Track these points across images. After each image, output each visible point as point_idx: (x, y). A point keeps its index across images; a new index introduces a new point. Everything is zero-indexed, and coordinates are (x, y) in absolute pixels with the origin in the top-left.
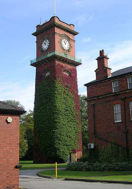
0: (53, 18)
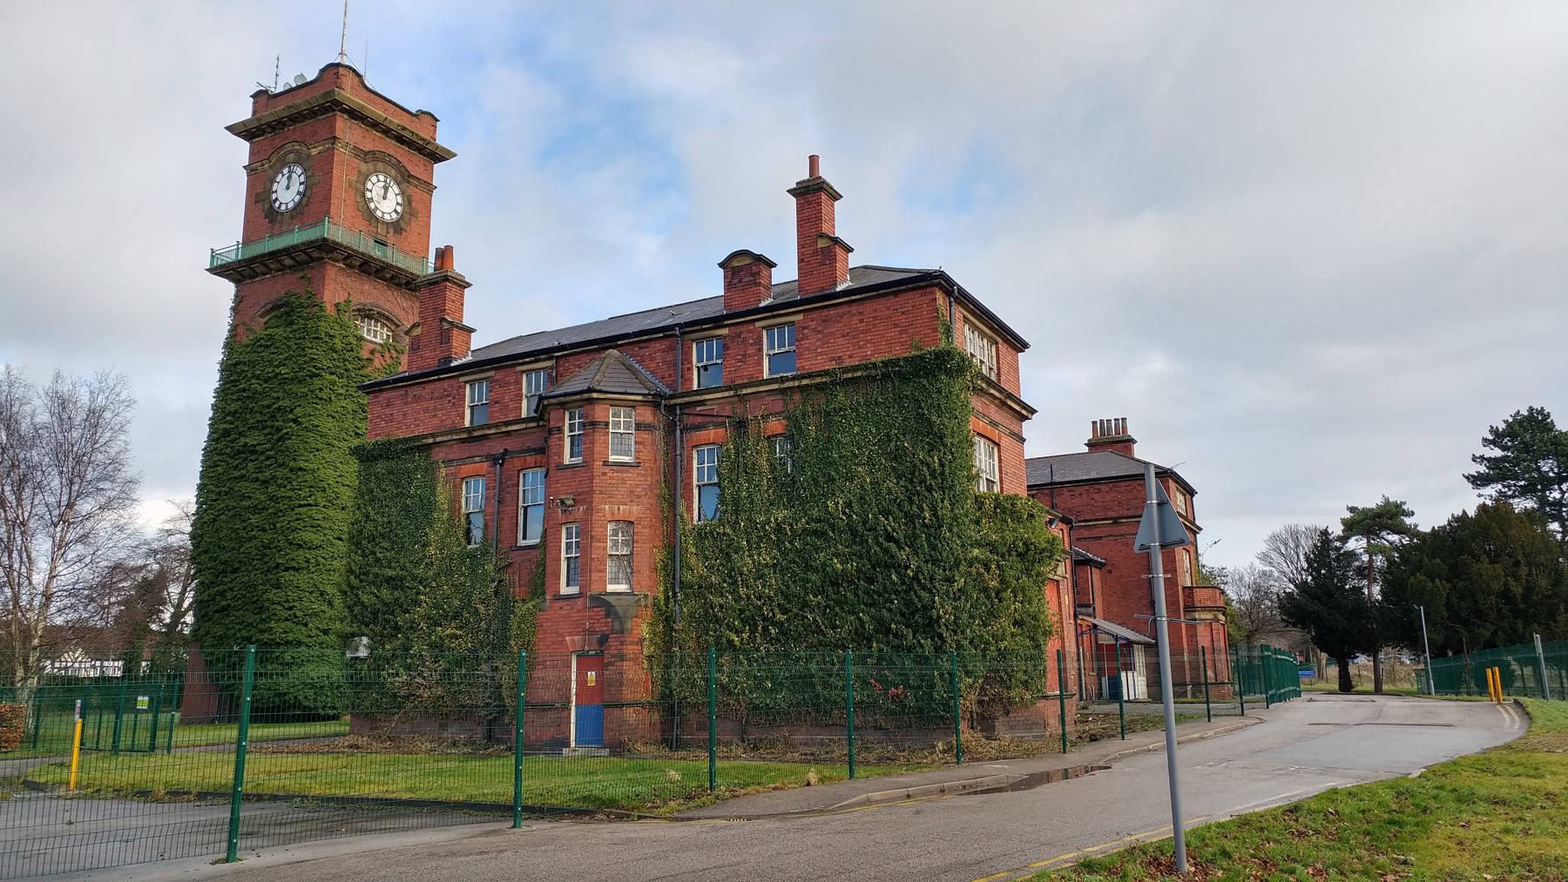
0: (332, 71)
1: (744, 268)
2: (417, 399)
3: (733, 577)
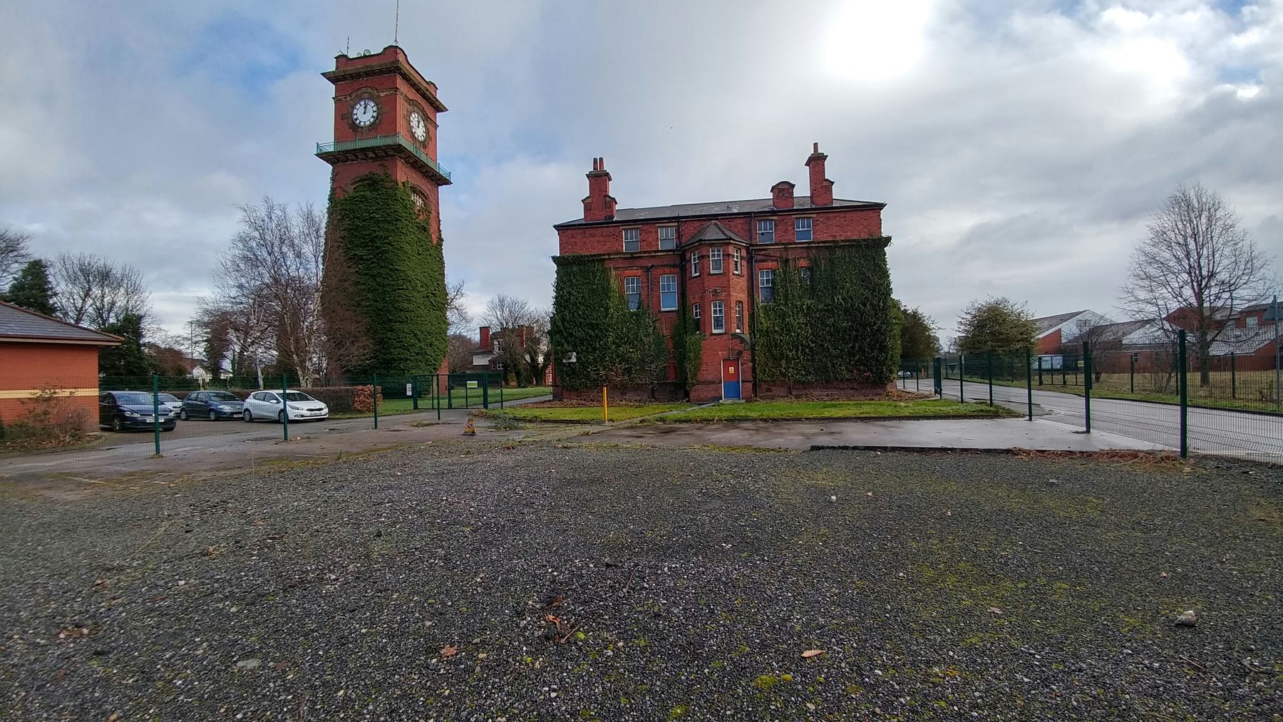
0: (393, 50)
1: (782, 190)
2: (593, 236)
3: (788, 328)
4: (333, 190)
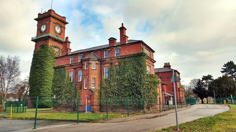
0: (50, 11)
4: (35, 49)
